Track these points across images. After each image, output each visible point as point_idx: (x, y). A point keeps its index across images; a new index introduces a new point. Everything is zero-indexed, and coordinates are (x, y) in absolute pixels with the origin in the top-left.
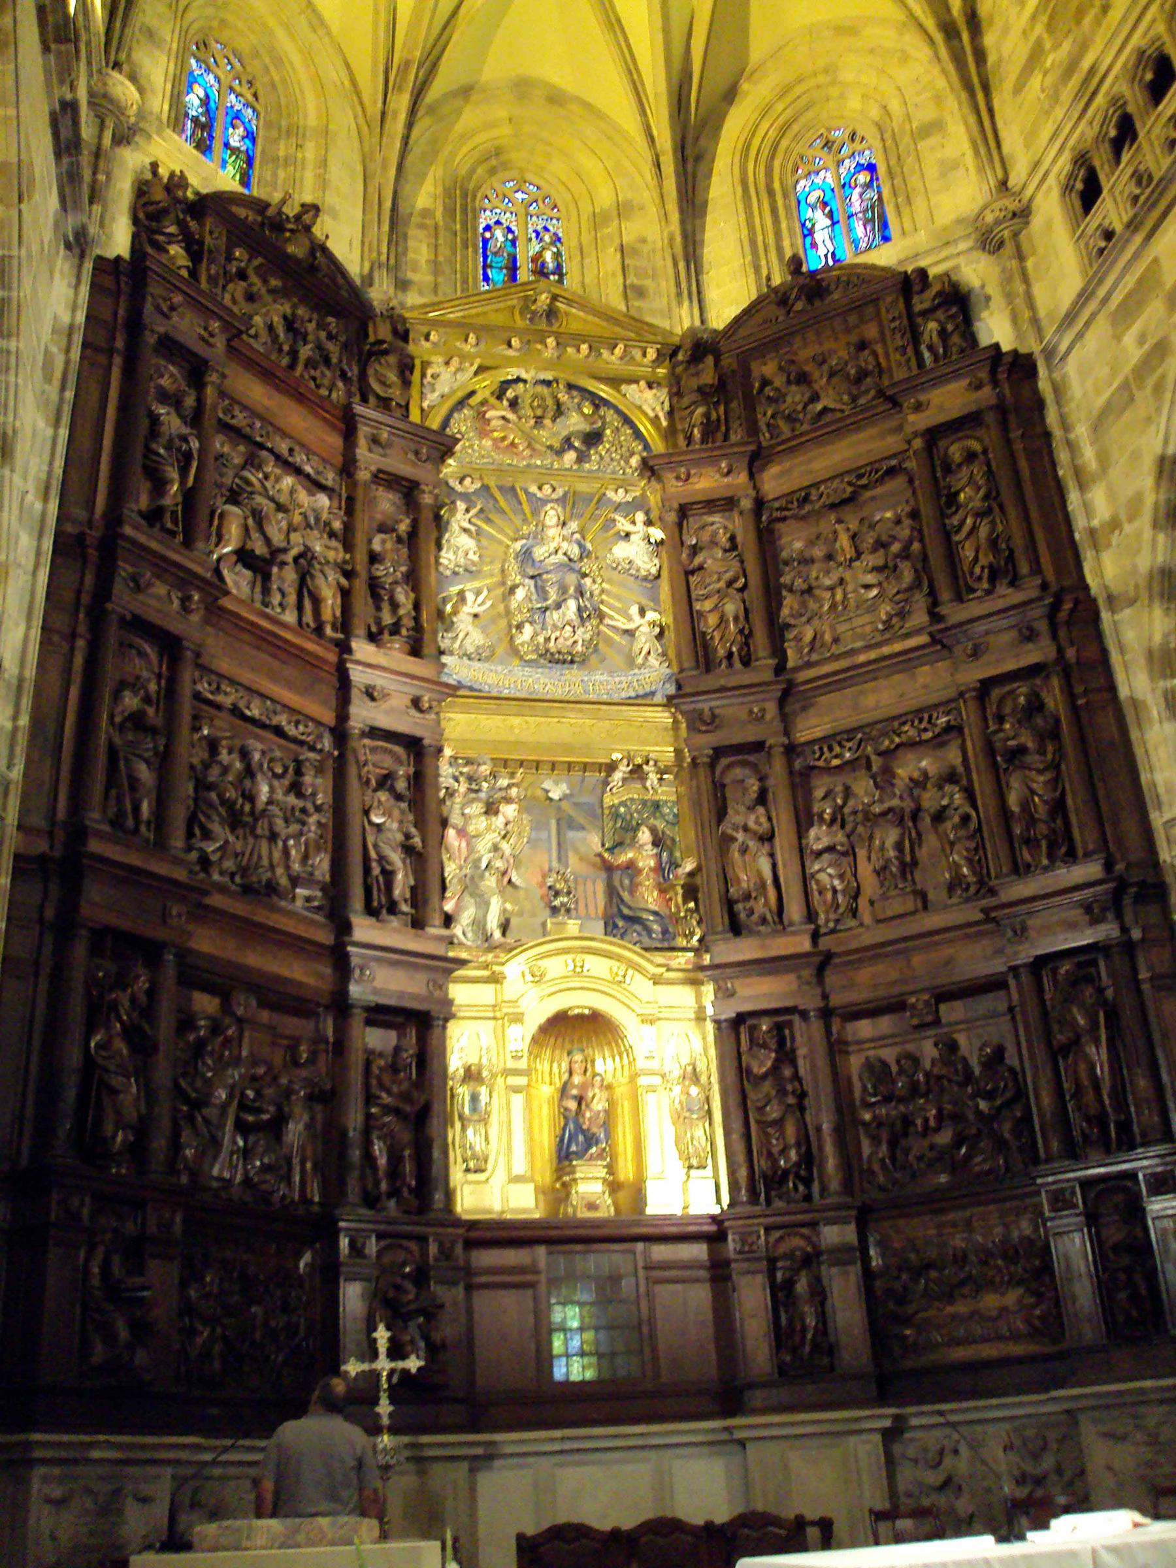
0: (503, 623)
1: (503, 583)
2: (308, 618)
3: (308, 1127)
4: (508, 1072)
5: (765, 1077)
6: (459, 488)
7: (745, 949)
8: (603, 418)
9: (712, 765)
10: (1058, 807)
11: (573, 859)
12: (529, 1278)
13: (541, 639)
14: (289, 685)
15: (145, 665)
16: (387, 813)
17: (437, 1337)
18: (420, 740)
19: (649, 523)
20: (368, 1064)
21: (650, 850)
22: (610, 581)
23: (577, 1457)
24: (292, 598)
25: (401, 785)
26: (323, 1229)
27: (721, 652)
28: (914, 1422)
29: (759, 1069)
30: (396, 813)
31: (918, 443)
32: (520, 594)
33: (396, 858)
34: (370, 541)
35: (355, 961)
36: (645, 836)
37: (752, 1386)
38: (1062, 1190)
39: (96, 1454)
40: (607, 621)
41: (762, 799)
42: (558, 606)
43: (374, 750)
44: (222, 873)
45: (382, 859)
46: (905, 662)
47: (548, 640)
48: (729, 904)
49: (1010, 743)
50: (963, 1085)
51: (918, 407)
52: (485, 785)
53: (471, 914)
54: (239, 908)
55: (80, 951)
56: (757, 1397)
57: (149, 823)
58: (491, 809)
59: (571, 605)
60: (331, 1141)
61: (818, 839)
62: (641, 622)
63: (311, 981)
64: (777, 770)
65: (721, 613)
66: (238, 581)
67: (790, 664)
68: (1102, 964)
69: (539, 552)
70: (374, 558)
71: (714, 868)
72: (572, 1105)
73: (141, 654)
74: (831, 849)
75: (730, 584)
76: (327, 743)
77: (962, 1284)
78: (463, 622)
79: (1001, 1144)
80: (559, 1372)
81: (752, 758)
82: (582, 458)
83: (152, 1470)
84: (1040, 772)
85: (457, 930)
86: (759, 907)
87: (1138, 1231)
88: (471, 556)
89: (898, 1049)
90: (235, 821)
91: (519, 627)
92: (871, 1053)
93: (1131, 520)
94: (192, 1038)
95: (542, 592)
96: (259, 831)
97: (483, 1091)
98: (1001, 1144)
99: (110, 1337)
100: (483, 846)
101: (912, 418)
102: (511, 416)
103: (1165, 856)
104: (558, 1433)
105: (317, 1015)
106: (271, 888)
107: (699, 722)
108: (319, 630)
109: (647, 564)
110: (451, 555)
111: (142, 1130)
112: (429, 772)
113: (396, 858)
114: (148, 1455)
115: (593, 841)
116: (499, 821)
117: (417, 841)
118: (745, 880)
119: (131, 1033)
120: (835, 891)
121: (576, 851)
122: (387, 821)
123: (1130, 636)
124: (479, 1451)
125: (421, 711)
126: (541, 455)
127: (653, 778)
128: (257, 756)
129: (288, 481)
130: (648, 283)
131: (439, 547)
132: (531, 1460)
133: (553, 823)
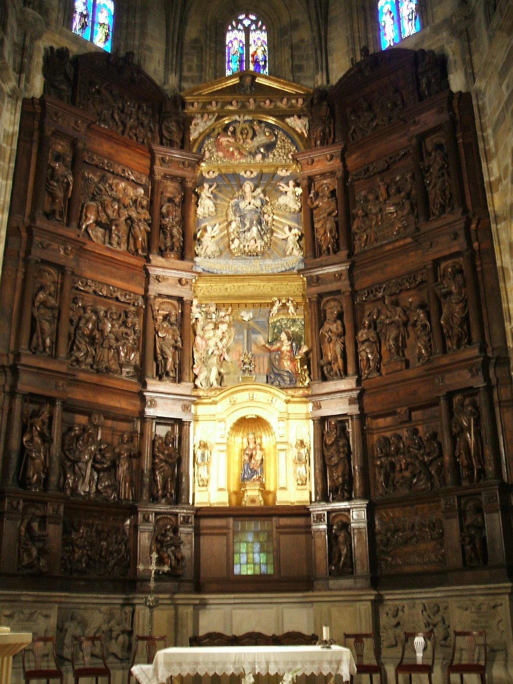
0: (226, 239)
1: (227, 220)
2: (132, 247)
3: (128, 469)
5: (332, 445)
6: (207, 176)
8: (276, 136)
9: (319, 302)
10: (466, 319)
11: (254, 348)
12: (225, 531)
13: (242, 246)
14: (122, 279)
15: (51, 277)
16: (167, 331)
17: (179, 556)
20: (153, 442)
22: (278, 215)
23: (240, 606)
24: (125, 239)
25: (173, 319)
26: (132, 511)
28: (387, 597)
30: (171, 331)
31: (414, 141)
32: (234, 225)
33: (169, 352)
34: (161, 207)
35: (148, 399)
36: (283, 336)
37: (317, 579)
38: (321, 514)
39: (23, 598)
40: (275, 235)
41: (340, 316)
42: (249, 230)
44: (86, 365)
46: (404, 250)
49: (443, 291)
50: (419, 449)
51: (415, 123)
52: (214, 316)
53: (207, 374)
54: (95, 379)
55: (18, 402)
56: (318, 584)
57: (50, 347)
58: (216, 327)
59: (254, 230)
60: (136, 474)
61: (362, 336)
62: (289, 234)
63: (130, 408)
64: (346, 303)
65: (324, 229)
66: (98, 233)
67: (356, 252)
68: (350, 421)
69: (242, 205)
70: (163, 216)
71: (315, 350)
72: (247, 458)
73: (50, 274)
74: (367, 340)
75: (329, 214)
76: (141, 302)
77: (411, 538)
79: (430, 477)
80: (237, 570)
81: (338, 297)
82: (264, 157)
83: (52, 605)
84: (457, 303)
85: (198, 383)
87: (480, 519)
89: (393, 432)
90: (92, 341)
91: (233, 241)
92: (383, 434)
93: (505, 179)
94: (73, 434)
96: (104, 345)
97: (207, 452)
98: (430, 477)
99: (30, 555)
100: (212, 343)
101: (412, 129)
103: (510, 344)
104: (232, 596)
105: (134, 421)
106: (108, 370)
107: (313, 281)
109: (295, 206)
110: (202, 210)
111: (47, 472)
112: (187, 311)
113: (169, 352)
114: (45, 599)
115: (261, 339)
116: (219, 332)
117: (179, 344)
118: (330, 356)
119: (42, 435)
120: (368, 359)
121: (256, 344)
122: (166, 335)
123: (503, 236)
124: (197, 602)
126: (245, 156)
127: (292, 309)
128: (102, 313)
129: (123, 185)
130: (304, 63)
132: (222, 606)
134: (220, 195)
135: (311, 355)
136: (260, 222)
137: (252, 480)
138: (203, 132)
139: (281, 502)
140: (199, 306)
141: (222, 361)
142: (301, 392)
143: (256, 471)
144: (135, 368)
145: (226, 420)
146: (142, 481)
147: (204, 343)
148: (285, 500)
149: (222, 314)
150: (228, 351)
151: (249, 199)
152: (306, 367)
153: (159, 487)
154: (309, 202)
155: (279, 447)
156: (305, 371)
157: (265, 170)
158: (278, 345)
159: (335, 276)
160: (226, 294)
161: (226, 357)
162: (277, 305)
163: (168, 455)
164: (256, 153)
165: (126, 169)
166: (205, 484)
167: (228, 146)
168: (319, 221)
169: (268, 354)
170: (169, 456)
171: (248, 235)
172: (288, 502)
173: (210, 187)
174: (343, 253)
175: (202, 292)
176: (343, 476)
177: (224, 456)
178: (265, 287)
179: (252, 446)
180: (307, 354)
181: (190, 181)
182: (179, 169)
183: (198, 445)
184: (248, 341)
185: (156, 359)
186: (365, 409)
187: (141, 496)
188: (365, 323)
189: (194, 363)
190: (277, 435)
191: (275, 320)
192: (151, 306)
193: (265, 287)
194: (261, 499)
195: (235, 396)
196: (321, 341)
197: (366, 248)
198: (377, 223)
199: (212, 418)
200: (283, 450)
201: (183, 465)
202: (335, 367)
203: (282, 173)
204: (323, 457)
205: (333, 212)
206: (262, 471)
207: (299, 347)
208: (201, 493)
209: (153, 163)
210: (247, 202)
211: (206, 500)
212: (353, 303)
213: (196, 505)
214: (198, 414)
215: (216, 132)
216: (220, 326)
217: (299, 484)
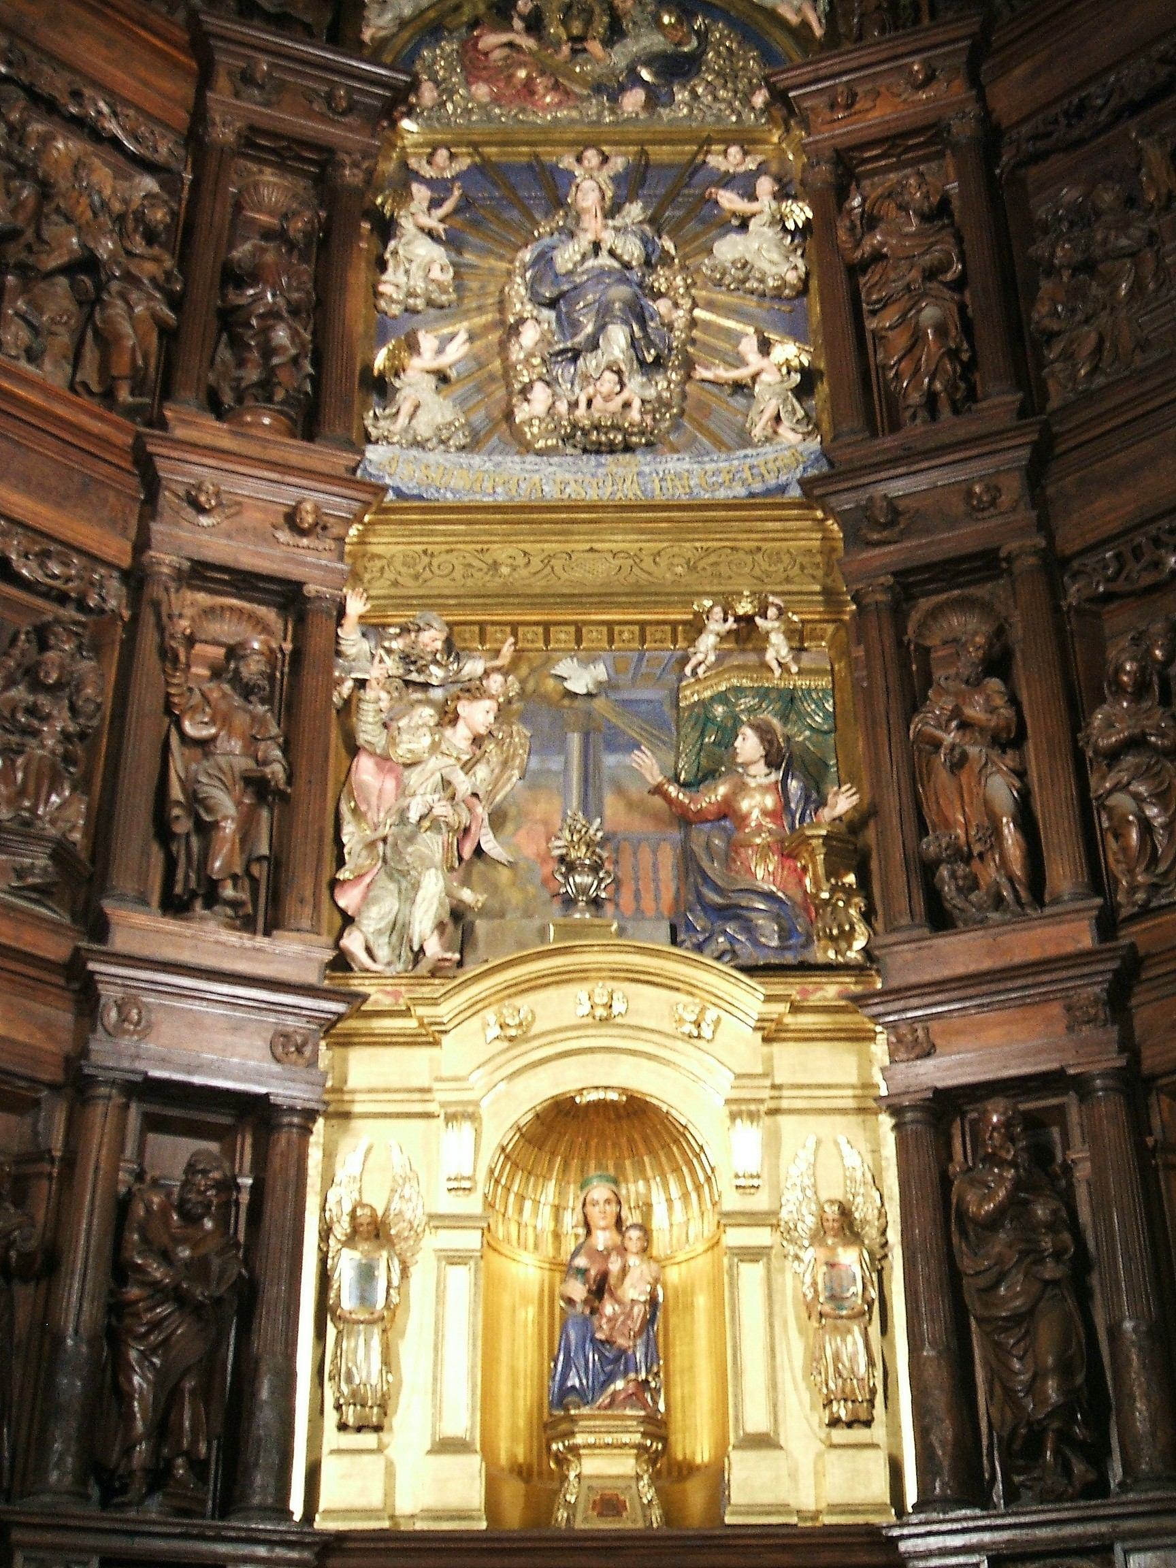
2: (89, 374)
4: (440, 1221)
5: (992, 1223)
7: (960, 953)
8: (702, 36)
9: (898, 611)
11: (611, 803)
13: (562, 407)
16: (223, 719)
18: (300, 585)
19: (782, 194)
20: (122, 1207)
21: (760, 775)
22: (710, 306)
24: (64, 339)
27: (915, 398)
29: (982, 1204)
32: (530, 335)
33: (226, 807)
35: (109, 993)
36: (748, 745)
41: (997, 663)
42: (593, 344)
43: (210, 612)
45: (195, 800)
47: (574, 405)
48: (927, 870)
53: (393, 908)
58: (448, 717)
65: (916, 327)
68: (1074, 1116)
69: (567, 256)
71: (891, 802)
74: (1135, 743)
76: (115, 597)
78: (415, 385)
82: (654, 99)
85: (353, 942)
86: (990, 873)
88: (436, 273)
91: (526, 390)
95: (568, 324)
102: (527, 42)
107: (862, 527)
108: (108, 396)
112: (317, 642)
113: (226, 807)
115: (648, 765)
116: (459, 737)
117: (277, 771)
118: (961, 825)
120: (1146, 826)
121: (620, 791)
122: (219, 750)
125: (303, 533)
127: (778, 647)
131: (382, 266)
133: (575, 740)
134: (472, 238)
135: (870, 835)
136: (637, 314)
137: (604, 1399)
138: (413, 19)
139: (750, 1510)
140: (373, 628)
141: (469, 862)
142: (830, 990)
143: (622, 1352)
144: (61, 853)
145: (484, 1111)
146: (50, 1385)
147: (390, 784)
148: (766, 1498)
149: (474, 667)
150: (498, 820)
151: (593, 226)
152: (851, 879)
153: (139, 1426)
154: (842, 235)
155: (736, 1237)
156: (848, 891)
157: (661, 153)
158: (722, 790)
159: (970, 494)
160: (494, 584)
161: (490, 845)
162: (717, 625)
163: (189, 1264)
164: (622, 89)
165: (88, 92)
166: (371, 1418)
167: (510, 65)
168: (885, 303)
169: (676, 835)
170: (198, 1268)
171: (590, 363)
172: (784, 1509)
173: (435, 204)
174: (999, 402)
175: (390, 575)
176: (1065, 1369)
177: (460, 1279)
178: (666, 559)
179: (602, 1239)
180: (855, 824)
181: (355, 165)
182: (310, 114)
183: (341, 1229)
184: (585, 779)
185: (163, 832)
186: (1146, 1053)
187: (41, 1470)
188: (1119, 669)
189: (341, 862)
190: (724, 1183)
191: (707, 694)
192: (156, 605)
193: (663, 561)
194: (649, 1494)
195: (525, 1003)
196: (917, 759)
197: (1100, 381)
198: (1137, 288)
199: (416, 1108)
200: (752, 1254)
201: (267, 1327)
202: (990, 873)
203: (731, 160)
204: (953, 1279)
205: (944, 267)
206: (652, 1356)
207: (815, 798)
208: (346, 1460)
209: (205, 80)
210: (584, 241)
211: (375, 1499)
212: (1057, 609)
213: (320, 1524)
214: (352, 1084)
215: (466, 14)
216: (464, 708)
217: (834, 1422)
